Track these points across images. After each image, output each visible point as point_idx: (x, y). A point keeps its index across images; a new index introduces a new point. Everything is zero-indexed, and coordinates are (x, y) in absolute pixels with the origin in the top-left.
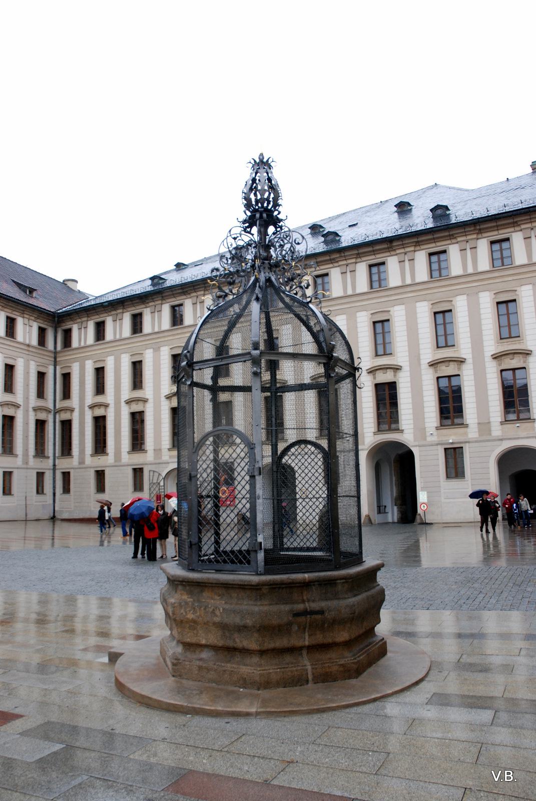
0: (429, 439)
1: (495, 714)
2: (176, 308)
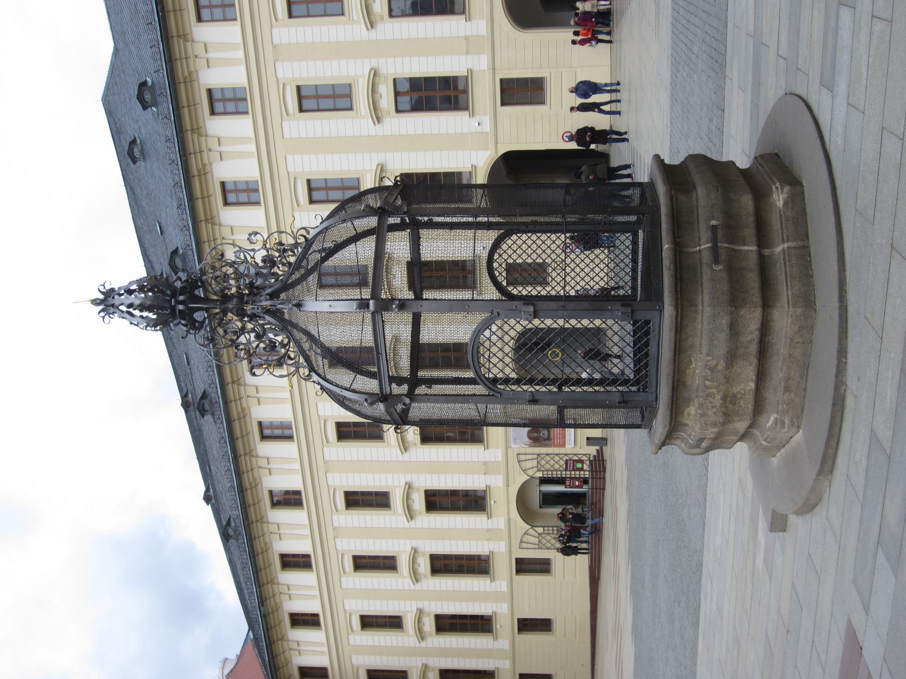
0: (487, 127)
1: (844, 5)
2: (275, 502)
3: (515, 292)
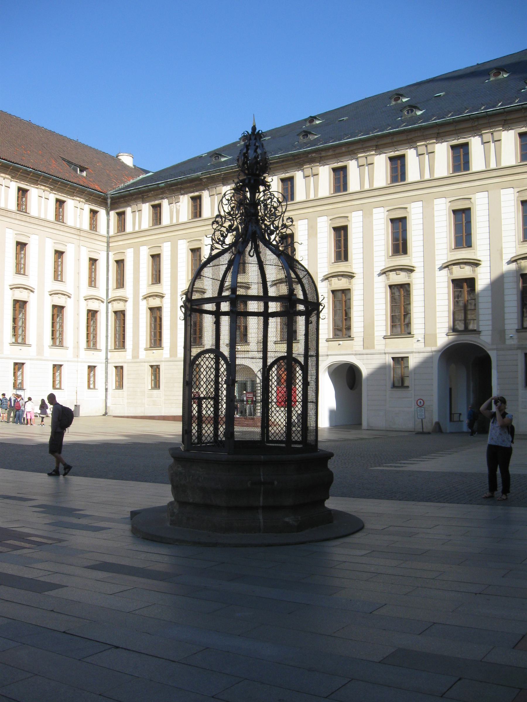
3: (274, 369)
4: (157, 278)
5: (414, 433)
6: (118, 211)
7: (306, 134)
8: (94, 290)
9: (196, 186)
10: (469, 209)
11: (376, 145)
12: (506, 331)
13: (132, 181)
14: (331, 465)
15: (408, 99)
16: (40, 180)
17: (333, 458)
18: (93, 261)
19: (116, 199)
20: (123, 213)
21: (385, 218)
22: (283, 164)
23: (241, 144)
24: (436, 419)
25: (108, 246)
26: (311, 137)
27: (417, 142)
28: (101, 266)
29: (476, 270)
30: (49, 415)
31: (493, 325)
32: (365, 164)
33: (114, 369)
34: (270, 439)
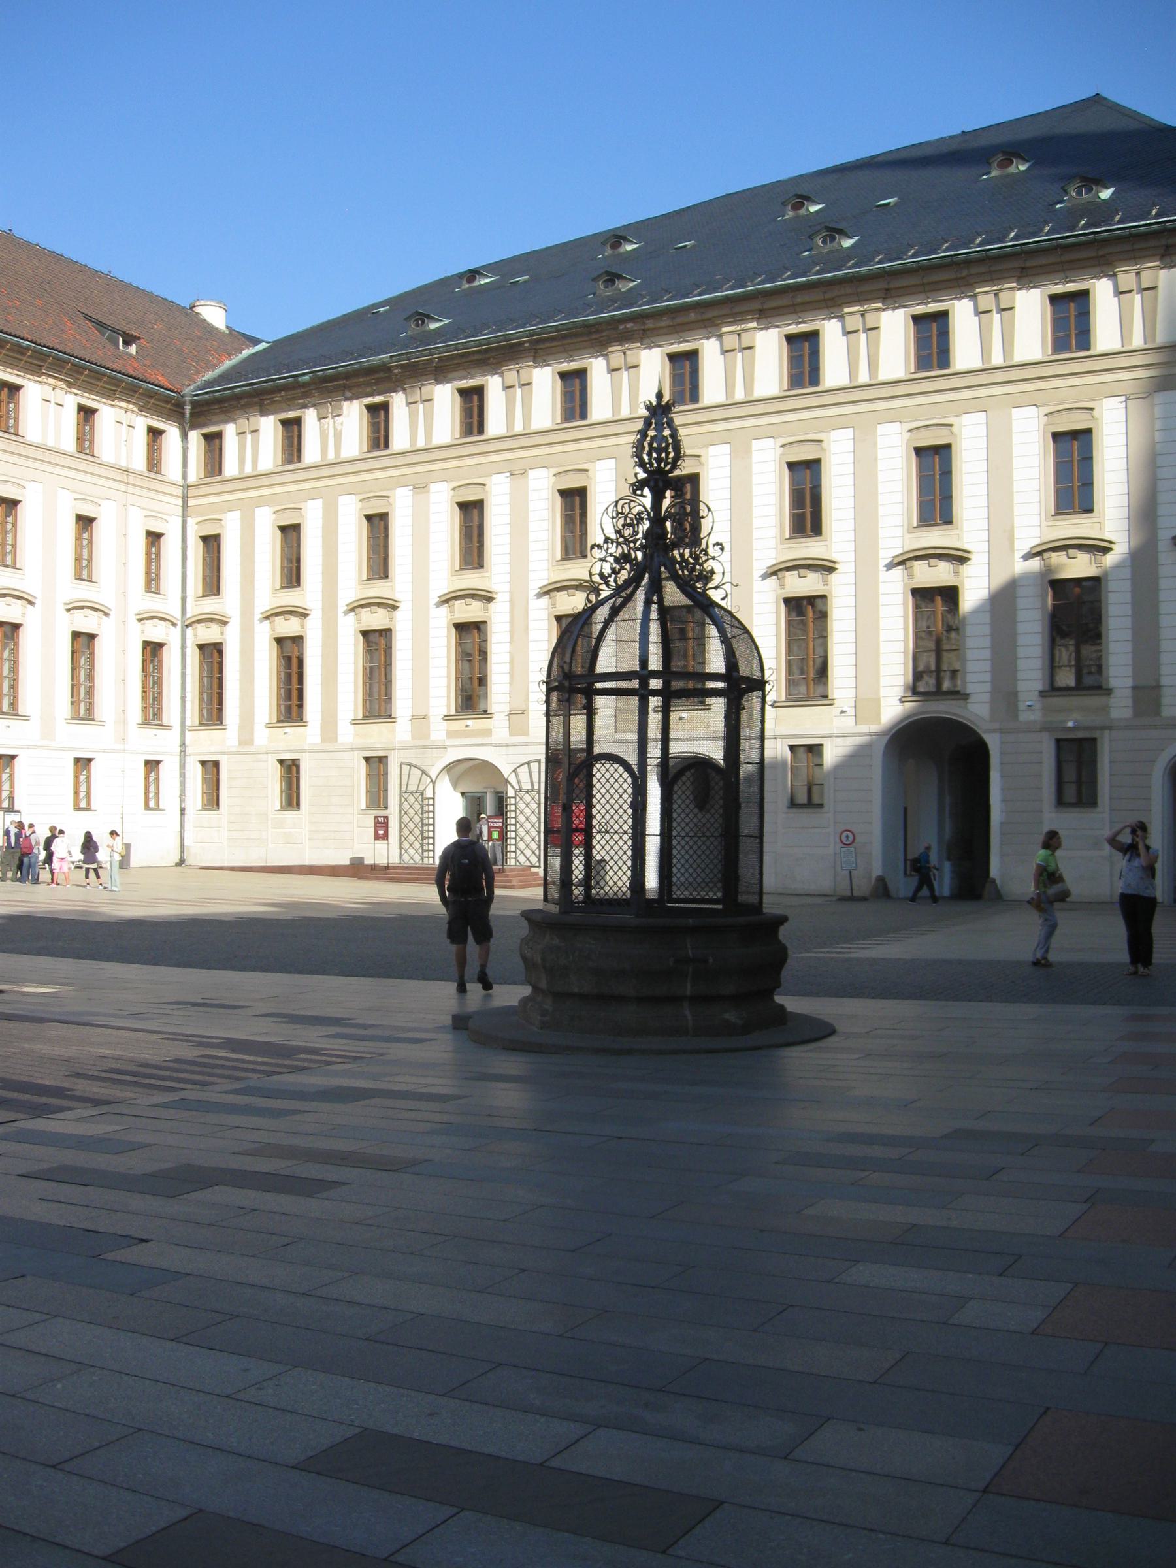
4: (292, 575)
5: (834, 899)
6: (206, 430)
7: (612, 278)
8: (160, 600)
9: (378, 382)
10: (948, 447)
11: (761, 310)
12: (1020, 694)
13: (228, 364)
14: (783, 932)
15: (821, 206)
16: (46, 365)
17: (786, 925)
18: (154, 537)
19: (203, 405)
20: (219, 435)
21: (778, 460)
22: (565, 342)
23: (463, 287)
24: (877, 871)
25: (185, 507)
26: (624, 286)
27: (844, 305)
28: (170, 548)
29: (960, 571)
30: (103, 866)
31: (993, 682)
32: (737, 347)
33: (199, 767)
34: (674, 896)
